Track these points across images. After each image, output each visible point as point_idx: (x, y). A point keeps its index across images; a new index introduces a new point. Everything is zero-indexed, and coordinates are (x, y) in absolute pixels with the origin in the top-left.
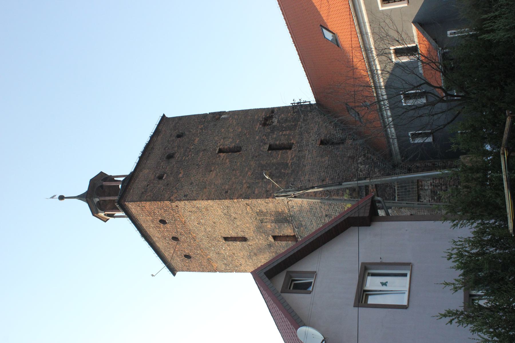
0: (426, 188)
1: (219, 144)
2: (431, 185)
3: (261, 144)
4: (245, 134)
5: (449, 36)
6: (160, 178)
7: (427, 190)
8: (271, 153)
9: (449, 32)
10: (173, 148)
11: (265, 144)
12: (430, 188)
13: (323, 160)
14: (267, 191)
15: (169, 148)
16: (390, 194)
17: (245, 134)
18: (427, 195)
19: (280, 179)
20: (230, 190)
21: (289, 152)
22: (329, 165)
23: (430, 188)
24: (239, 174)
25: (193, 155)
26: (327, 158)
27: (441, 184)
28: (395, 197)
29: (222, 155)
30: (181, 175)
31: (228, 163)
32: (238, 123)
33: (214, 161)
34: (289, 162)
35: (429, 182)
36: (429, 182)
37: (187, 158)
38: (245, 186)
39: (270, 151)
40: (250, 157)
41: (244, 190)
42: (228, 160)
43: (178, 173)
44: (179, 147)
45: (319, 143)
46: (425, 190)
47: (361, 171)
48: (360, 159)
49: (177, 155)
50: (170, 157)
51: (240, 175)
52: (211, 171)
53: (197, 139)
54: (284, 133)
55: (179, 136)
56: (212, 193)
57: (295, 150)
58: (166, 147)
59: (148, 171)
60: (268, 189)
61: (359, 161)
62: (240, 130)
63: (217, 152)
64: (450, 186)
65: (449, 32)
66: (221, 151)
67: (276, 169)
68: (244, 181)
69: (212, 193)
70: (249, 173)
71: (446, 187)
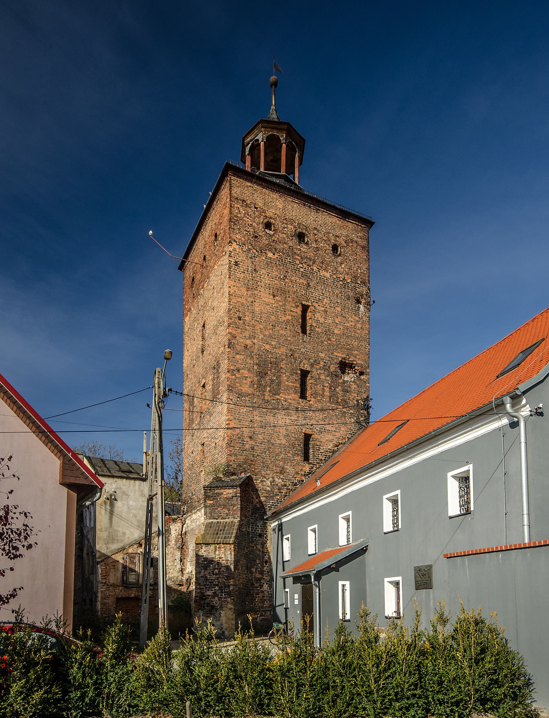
0: (217, 553)
1: (316, 305)
2: (220, 558)
3: (312, 361)
4: (329, 339)
5: (341, 583)
6: (268, 226)
7: (215, 554)
8: (297, 373)
9: (347, 583)
10: (316, 241)
11: (312, 365)
12: (217, 557)
13: (282, 438)
14: (239, 371)
15: (315, 235)
16: (220, 513)
17: (329, 339)
18: (209, 553)
19: (255, 386)
20: (244, 323)
21: (297, 396)
22: (273, 444)
23: (217, 557)
24: (267, 333)
25: (302, 270)
26: (284, 442)
27: (220, 569)
28: (217, 519)
29: (299, 310)
30: (270, 255)
31: (284, 319)
32: (347, 329)
33: (290, 299)
34: (282, 397)
35: (223, 556)
36: (223, 556)
37: (298, 262)
38: (248, 342)
39: (300, 372)
40: (292, 347)
41: (241, 340)
42: (290, 318)
43: (275, 251)
44: (317, 249)
45: (307, 432)
46: (215, 551)
47: (262, 481)
48: (280, 480)
49: (304, 248)
50: (301, 237)
51: (265, 336)
52: (274, 296)
53: (328, 275)
54: (327, 389)
55: (335, 248)
56: (240, 300)
57: (299, 403)
58: (318, 231)
59: (281, 206)
60: (241, 371)
61: (277, 480)
62: (336, 331)
63: (304, 303)
64: (218, 578)
65: (347, 583)
66: (305, 308)
67: (272, 381)
68: (256, 341)
69: (240, 300)
70: (267, 347)
71: (216, 574)
